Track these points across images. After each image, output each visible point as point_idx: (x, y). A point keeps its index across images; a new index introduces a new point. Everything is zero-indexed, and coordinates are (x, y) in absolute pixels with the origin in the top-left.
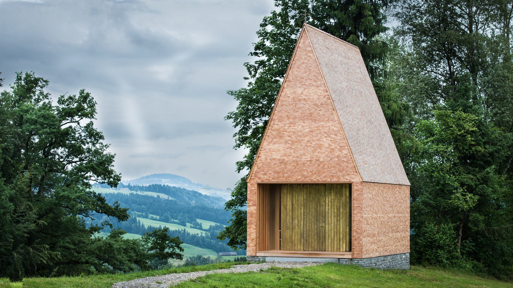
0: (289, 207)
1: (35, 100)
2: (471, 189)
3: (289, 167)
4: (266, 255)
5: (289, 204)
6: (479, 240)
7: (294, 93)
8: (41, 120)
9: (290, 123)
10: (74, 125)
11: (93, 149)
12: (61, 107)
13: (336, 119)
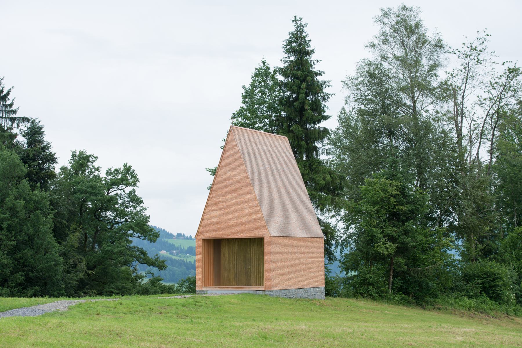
0: (227, 255)
1: (88, 173)
2: (393, 239)
3: (223, 227)
4: (208, 289)
5: (227, 253)
6: (407, 279)
7: (225, 174)
8: (89, 190)
9: (223, 196)
10: (119, 192)
11: (134, 211)
12: (109, 177)
13: (253, 192)
